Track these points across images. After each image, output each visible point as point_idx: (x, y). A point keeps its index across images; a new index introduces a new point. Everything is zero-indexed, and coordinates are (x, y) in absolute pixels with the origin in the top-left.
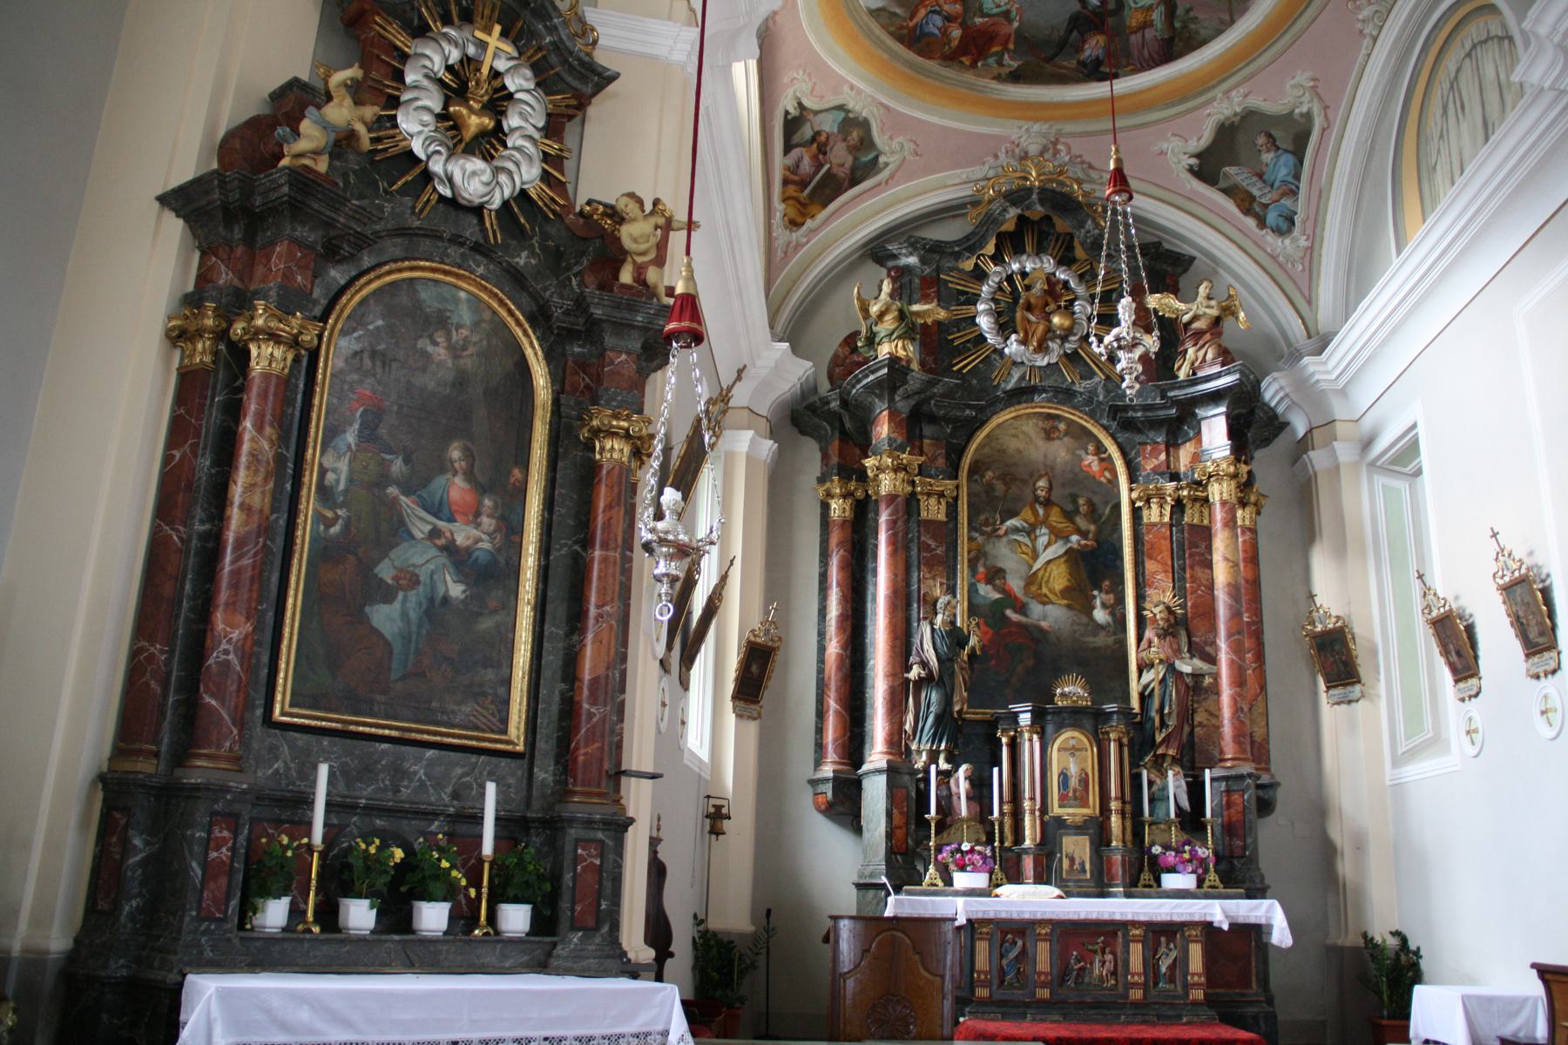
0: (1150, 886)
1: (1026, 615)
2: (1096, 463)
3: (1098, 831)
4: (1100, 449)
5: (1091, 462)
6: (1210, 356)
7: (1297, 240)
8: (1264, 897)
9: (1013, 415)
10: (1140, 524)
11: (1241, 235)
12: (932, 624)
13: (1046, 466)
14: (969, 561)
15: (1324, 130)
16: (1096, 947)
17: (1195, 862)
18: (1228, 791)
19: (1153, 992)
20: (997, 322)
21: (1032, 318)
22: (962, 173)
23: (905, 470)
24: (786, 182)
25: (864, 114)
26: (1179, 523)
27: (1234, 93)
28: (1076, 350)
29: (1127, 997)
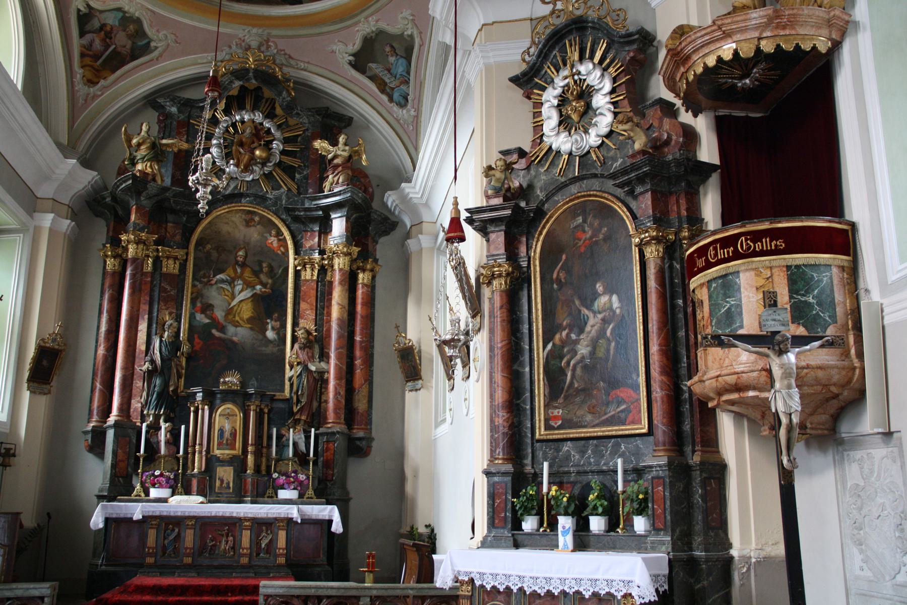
1: (224, 333)
2: (276, 241)
3: (239, 464)
4: (279, 233)
5: (273, 241)
6: (341, 180)
12: (161, 337)
15: (420, 46)
16: (224, 533)
17: (296, 483)
23: (144, 243)
24: (83, 55)
25: (137, 15)
26: (323, 280)
27: (370, 19)
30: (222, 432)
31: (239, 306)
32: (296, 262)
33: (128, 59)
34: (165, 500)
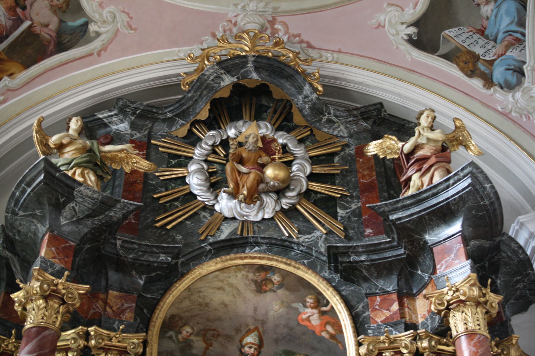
9: (219, 266)
13: (256, 320)
20: (207, 179)
21: (243, 169)
22: (182, 51)
28: (294, 205)
33: (52, 47)
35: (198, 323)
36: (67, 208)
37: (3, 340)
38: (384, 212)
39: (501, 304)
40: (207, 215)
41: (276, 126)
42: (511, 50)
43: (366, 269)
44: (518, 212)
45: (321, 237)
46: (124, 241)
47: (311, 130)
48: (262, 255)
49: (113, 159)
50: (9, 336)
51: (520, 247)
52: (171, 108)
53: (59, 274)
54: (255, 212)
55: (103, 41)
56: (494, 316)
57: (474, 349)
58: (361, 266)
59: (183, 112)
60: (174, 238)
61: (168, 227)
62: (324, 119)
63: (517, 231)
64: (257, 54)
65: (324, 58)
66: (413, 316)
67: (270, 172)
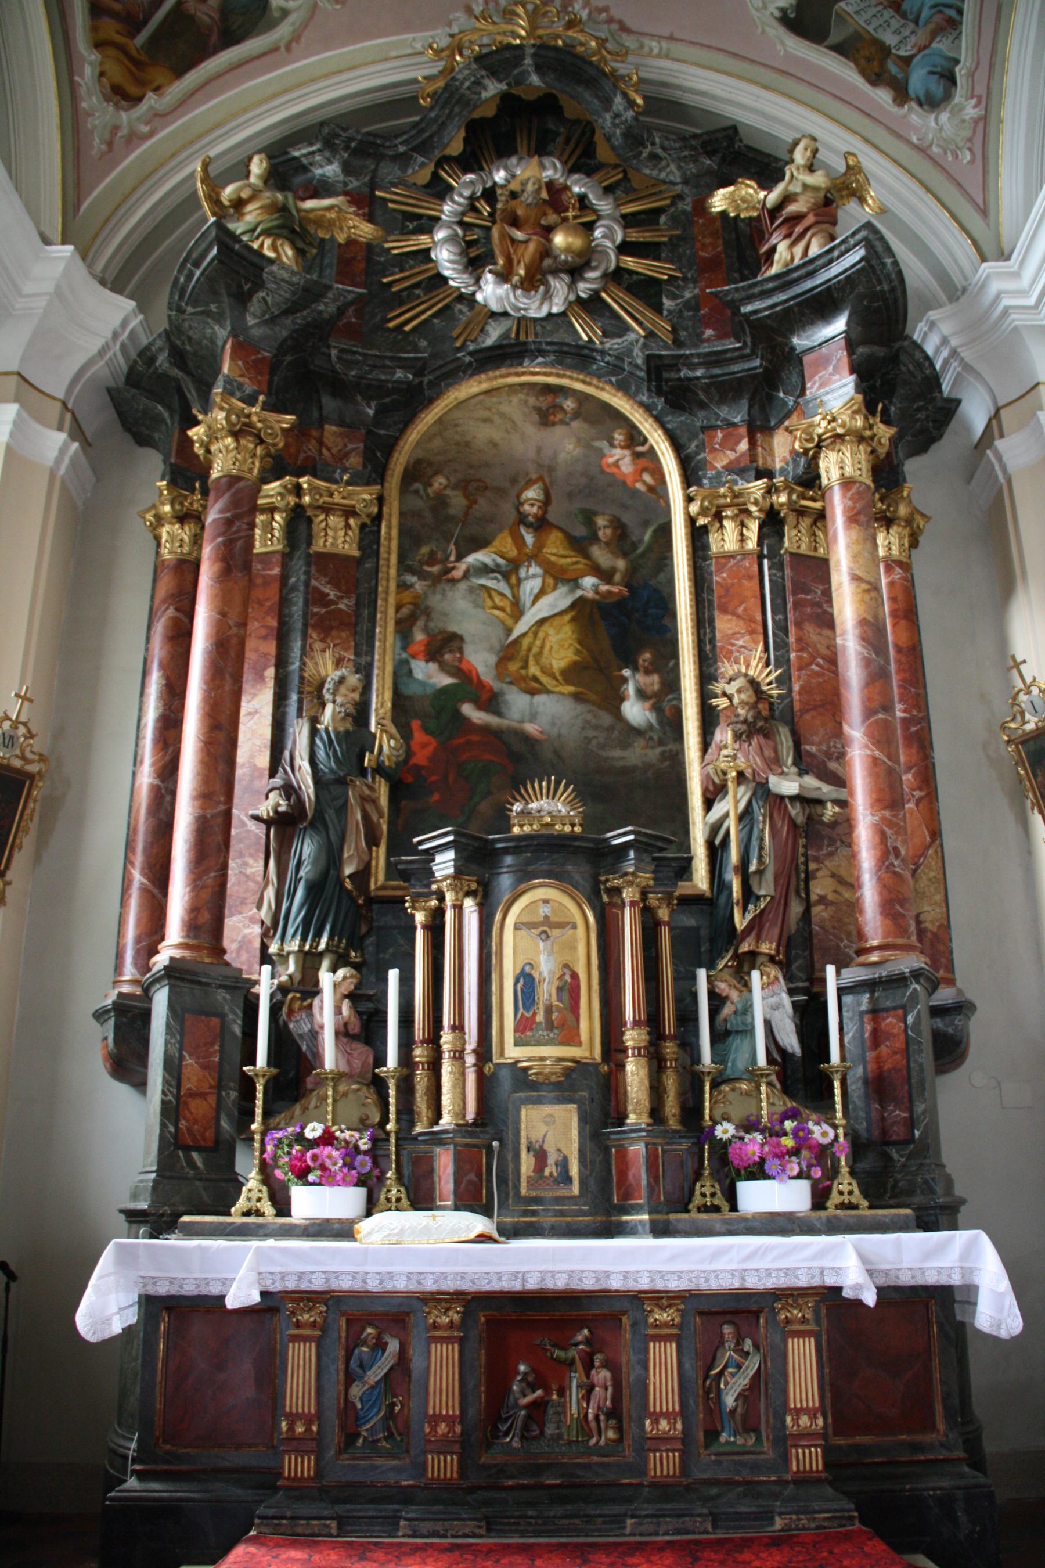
0: (716, 1209)
1: (498, 713)
4: (635, 438)
7: (961, 108)
8: (954, 1226)
9: (485, 386)
10: (706, 558)
11: (866, 121)
12: (314, 721)
13: (540, 466)
14: (398, 622)
16: (572, 1353)
17: (805, 1154)
18: (875, 1012)
19: (706, 1457)
20: (463, 253)
21: (519, 235)
22: (417, 39)
29: (643, 1471)
30: (527, 982)
31: (536, 635)
32: (694, 508)
34: (343, 1230)
35: (456, 471)
36: (255, 300)
37: (186, 497)
38: (733, 301)
39: (894, 441)
40: (465, 309)
41: (570, 164)
42: (939, 39)
43: (703, 390)
44: (929, 304)
45: (637, 341)
46: (342, 351)
47: (625, 172)
48: (548, 370)
49: (319, 222)
50: (193, 491)
51: (927, 358)
52: (405, 137)
53: (251, 400)
54: (537, 303)
55: (293, 24)
56: (882, 456)
57: (850, 503)
58: (696, 386)
59: (424, 143)
60: (416, 346)
61: (407, 328)
62: (645, 153)
63: (925, 334)
64: (538, 42)
65: (646, 49)
66: (769, 459)
67: (559, 240)
